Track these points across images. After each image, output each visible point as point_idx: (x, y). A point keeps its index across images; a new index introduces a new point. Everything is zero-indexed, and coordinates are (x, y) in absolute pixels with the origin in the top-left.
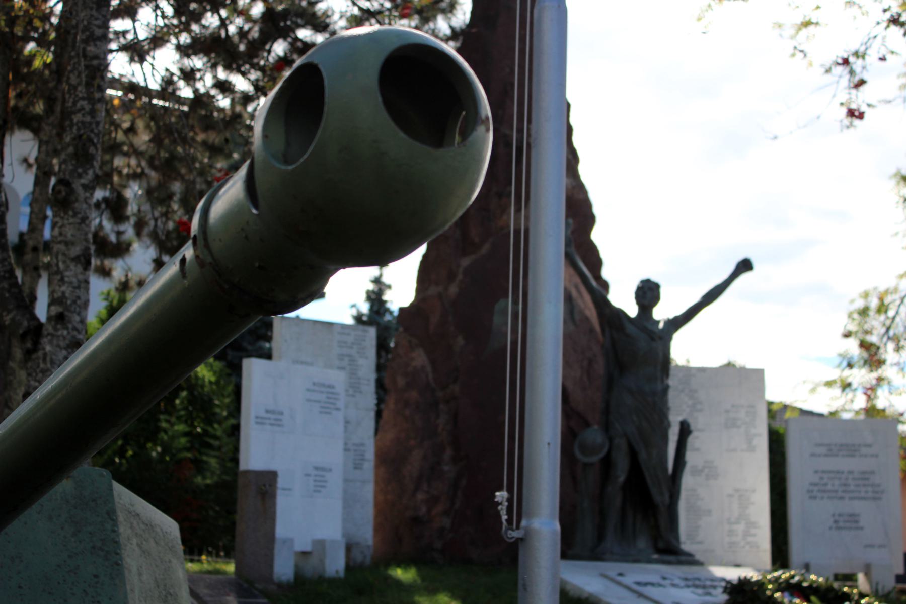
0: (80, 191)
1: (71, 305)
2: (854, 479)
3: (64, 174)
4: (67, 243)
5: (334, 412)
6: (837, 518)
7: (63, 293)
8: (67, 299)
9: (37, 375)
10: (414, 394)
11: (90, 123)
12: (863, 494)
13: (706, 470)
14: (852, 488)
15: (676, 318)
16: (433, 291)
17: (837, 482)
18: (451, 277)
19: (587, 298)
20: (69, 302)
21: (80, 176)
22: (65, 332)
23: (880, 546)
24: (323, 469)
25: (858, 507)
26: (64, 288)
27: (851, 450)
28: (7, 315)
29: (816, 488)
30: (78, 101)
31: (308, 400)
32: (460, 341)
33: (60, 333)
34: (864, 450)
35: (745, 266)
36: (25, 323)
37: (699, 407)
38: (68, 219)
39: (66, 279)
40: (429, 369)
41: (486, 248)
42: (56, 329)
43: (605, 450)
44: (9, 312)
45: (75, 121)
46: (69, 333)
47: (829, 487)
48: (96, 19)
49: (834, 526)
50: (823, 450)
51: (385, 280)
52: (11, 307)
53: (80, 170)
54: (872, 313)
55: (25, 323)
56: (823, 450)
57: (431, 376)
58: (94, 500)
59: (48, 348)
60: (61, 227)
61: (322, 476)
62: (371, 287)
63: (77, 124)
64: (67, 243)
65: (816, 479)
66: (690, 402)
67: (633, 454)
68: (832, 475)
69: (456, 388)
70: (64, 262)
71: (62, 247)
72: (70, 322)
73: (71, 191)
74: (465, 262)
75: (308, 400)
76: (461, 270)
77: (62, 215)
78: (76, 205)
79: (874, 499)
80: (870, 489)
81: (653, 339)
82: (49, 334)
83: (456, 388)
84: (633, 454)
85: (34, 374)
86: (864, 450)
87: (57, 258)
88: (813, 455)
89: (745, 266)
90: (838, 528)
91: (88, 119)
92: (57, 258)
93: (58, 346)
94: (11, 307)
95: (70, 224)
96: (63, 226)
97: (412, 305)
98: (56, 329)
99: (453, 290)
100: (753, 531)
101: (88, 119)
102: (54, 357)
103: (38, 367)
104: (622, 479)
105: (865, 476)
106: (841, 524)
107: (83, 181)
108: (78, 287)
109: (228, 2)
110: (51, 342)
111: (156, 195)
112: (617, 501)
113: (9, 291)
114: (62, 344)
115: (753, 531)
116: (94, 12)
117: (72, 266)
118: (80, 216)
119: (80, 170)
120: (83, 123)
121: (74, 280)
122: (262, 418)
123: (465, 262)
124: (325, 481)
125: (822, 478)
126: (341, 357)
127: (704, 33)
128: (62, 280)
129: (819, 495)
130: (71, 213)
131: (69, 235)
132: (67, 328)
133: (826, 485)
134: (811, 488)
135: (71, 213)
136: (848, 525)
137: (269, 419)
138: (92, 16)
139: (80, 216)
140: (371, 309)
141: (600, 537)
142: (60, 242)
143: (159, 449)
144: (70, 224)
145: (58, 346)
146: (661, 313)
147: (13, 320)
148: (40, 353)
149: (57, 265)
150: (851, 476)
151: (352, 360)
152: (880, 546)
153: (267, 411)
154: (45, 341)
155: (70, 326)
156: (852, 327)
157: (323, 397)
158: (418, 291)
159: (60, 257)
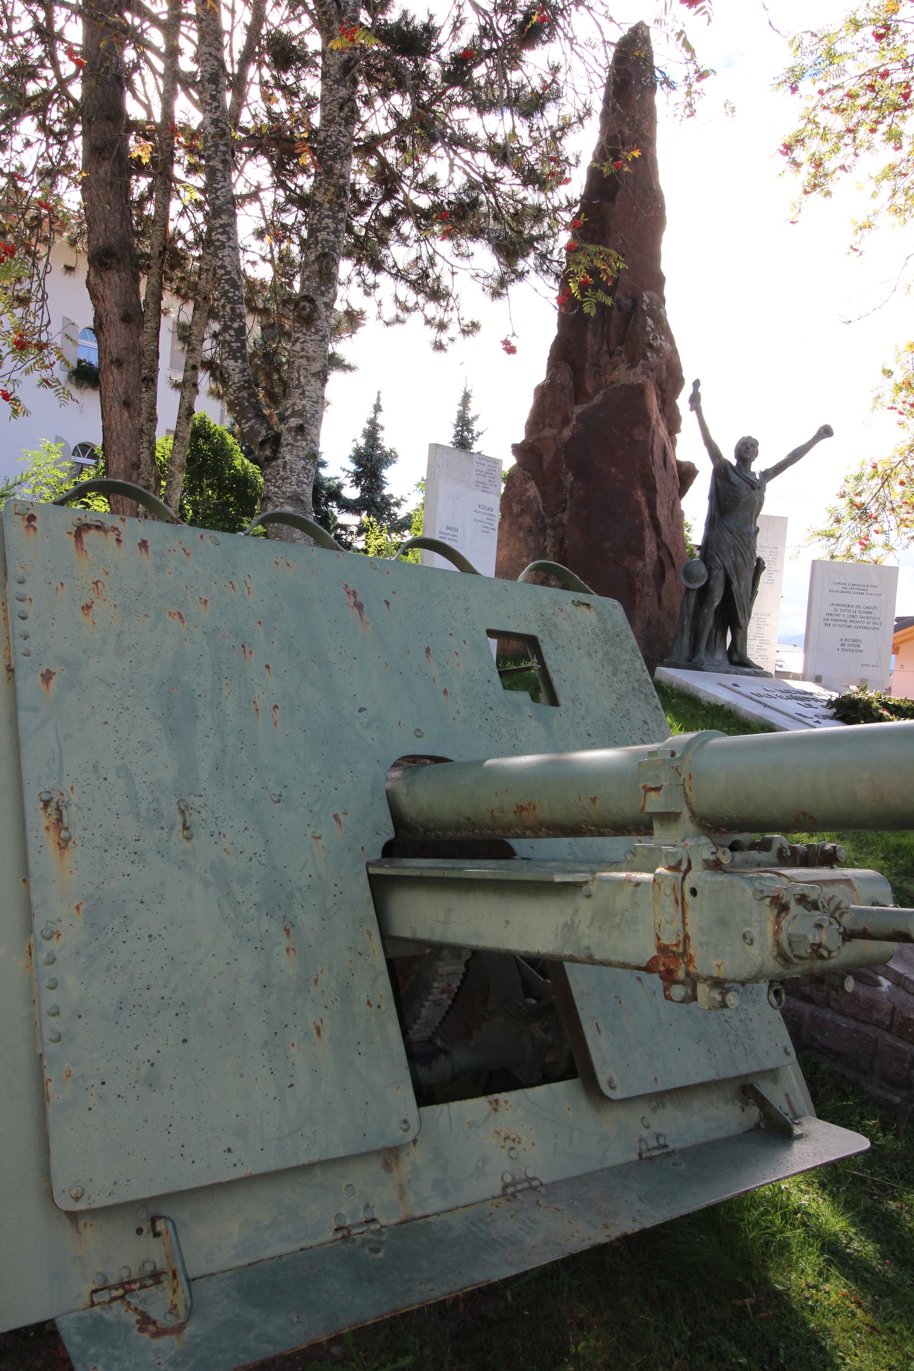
0: (322, 308)
1: (310, 418)
3: (308, 290)
4: (308, 359)
6: (844, 642)
7: (304, 406)
8: (307, 412)
9: (276, 481)
10: (527, 520)
11: (334, 242)
12: (865, 625)
14: (858, 619)
15: (767, 471)
16: (547, 432)
17: (847, 614)
18: (566, 421)
20: (308, 415)
21: (323, 294)
22: (304, 443)
23: (874, 666)
25: (860, 634)
26: (304, 402)
27: (861, 590)
28: (246, 423)
29: (830, 618)
30: (323, 219)
31: (475, 520)
32: (570, 477)
33: (299, 444)
34: (871, 590)
35: (826, 432)
36: (264, 432)
38: (310, 336)
39: (307, 393)
40: (539, 499)
41: (597, 399)
42: (296, 440)
43: (706, 579)
44: (248, 420)
45: (320, 238)
46: (307, 445)
47: (841, 618)
48: (344, 136)
49: (840, 648)
50: (840, 588)
51: (379, 421)
52: (250, 415)
53: (323, 288)
54: (864, 479)
55: (264, 432)
56: (840, 588)
57: (541, 505)
58: (618, 636)
59: (288, 457)
60: (302, 343)
62: (367, 426)
63: (321, 242)
64: (308, 359)
65: (831, 610)
67: (728, 583)
68: (843, 608)
69: (565, 517)
70: (305, 377)
71: (304, 362)
72: (309, 435)
73: (315, 309)
74: (578, 410)
75: (475, 520)
76: (575, 416)
77: (304, 331)
78: (319, 323)
79: (873, 629)
80: (871, 621)
81: (753, 488)
82: (288, 444)
83: (565, 517)
84: (728, 583)
85: (273, 481)
86: (871, 590)
87: (298, 372)
88: (830, 591)
89: (826, 432)
91: (332, 238)
92: (298, 372)
93: (298, 456)
94: (250, 415)
95: (312, 341)
96: (305, 342)
97: (523, 442)
98: (296, 440)
99: (567, 433)
100: (765, 646)
101: (332, 238)
102: (294, 466)
103: (278, 474)
104: (716, 604)
105: (869, 610)
106: (846, 647)
107: (325, 299)
108: (317, 402)
110: (290, 452)
111: (220, 338)
112: (710, 622)
113: (248, 401)
114: (301, 454)
115: (765, 646)
116: (342, 129)
117: (313, 380)
118: (321, 334)
119: (323, 288)
120: (327, 241)
121: (314, 395)
122: (444, 533)
123: (578, 410)
125: (836, 610)
127: (793, 222)
128: (303, 393)
129: (832, 623)
130: (313, 330)
131: (310, 350)
132: (306, 440)
134: (827, 617)
135: (313, 330)
136: (852, 648)
138: (340, 132)
139: (321, 334)
140: (367, 443)
141: (694, 648)
142: (302, 357)
144: (312, 341)
145: (298, 456)
146: (757, 466)
147: (252, 428)
148: (280, 461)
149: (299, 379)
150: (858, 610)
152: (874, 666)
153: (448, 528)
154: (284, 450)
155: (309, 438)
156: (849, 488)
159: (302, 372)
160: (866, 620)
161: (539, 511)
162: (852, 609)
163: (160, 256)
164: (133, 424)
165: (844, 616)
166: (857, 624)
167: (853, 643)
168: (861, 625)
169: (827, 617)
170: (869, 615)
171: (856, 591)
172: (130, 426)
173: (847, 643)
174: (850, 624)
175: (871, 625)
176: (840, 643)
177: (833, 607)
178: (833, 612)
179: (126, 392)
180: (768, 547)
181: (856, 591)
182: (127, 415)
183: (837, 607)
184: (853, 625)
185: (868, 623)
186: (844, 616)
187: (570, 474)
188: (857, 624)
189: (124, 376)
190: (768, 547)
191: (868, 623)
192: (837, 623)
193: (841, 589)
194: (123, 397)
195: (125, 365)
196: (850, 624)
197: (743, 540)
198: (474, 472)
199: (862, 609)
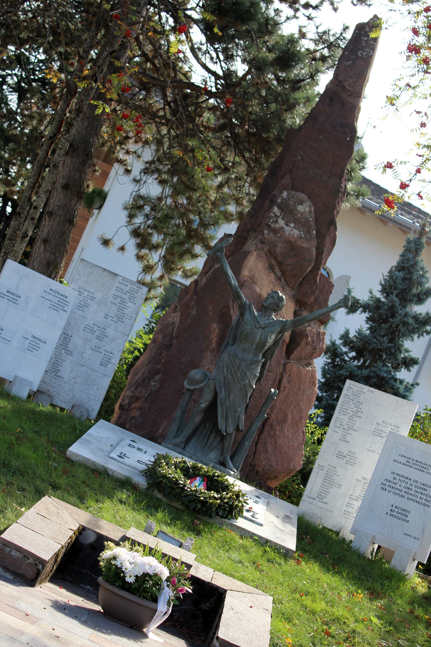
2: (415, 486)
5: (60, 311)
6: (394, 508)
12: (418, 499)
13: (348, 457)
14: (412, 492)
17: (403, 484)
19: (120, 293)
23: (415, 538)
24: (40, 340)
25: (410, 506)
29: (388, 484)
37: (359, 414)
47: (397, 486)
49: (389, 512)
50: (404, 460)
56: (404, 460)
61: (39, 344)
66: (355, 409)
68: (402, 478)
79: (424, 505)
80: (424, 497)
90: (392, 515)
106: (395, 514)
109: (430, 45)
124: (39, 348)
125: (394, 478)
126: (116, 297)
129: (388, 488)
133: (396, 484)
134: (385, 482)
136: (399, 516)
137: (9, 297)
143: (196, 521)
150: (415, 484)
151: (123, 301)
152: (415, 538)
157: (56, 300)
158: (328, 298)
160: (419, 496)
161: (172, 333)
162: (409, 482)
163: (50, 139)
164: (44, 255)
165: (400, 486)
166: (410, 496)
167: (402, 512)
168: (414, 498)
169: (385, 482)
170: (424, 492)
171: (418, 467)
172: (42, 256)
173: (396, 510)
174: (404, 494)
175: (423, 501)
176: (390, 508)
177: (393, 476)
178: (391, 479)
179: (48, 234)
180: (391, 425)
181: (418, 467)
182: (43, 248)
183: (397, 476)
184: (407, 496)
185: (421, 498)
186: (400, 486)
187: (195, 310)
188: (410, 496)
189: (51, 223)
190: (391, 425)
191: (421, 498)
192: (393, 490)
193: (405, 462)
194: (45, 237)
195: (54, 216)
196: (404, 494)
197: (235, 361)
198: (114, 288)
199: (419, 485)
